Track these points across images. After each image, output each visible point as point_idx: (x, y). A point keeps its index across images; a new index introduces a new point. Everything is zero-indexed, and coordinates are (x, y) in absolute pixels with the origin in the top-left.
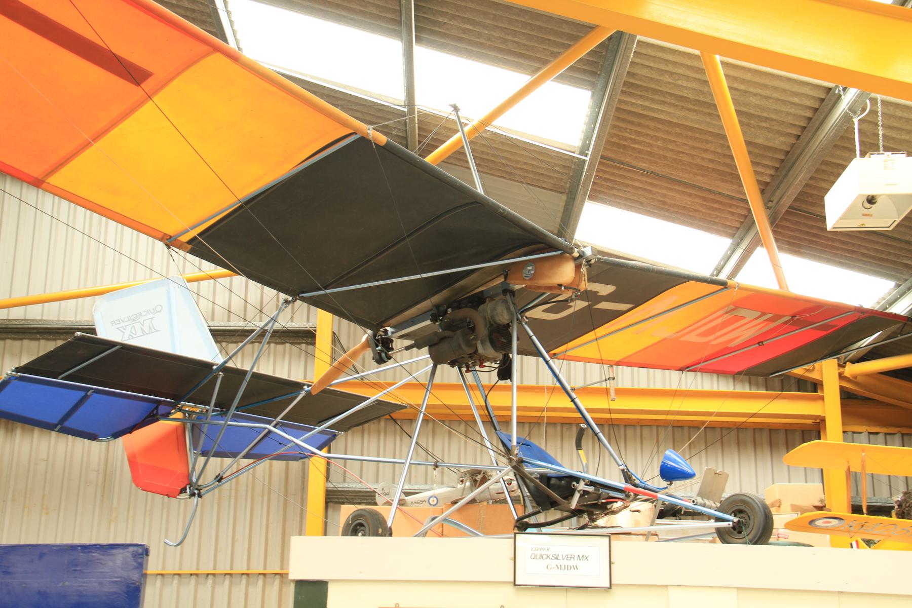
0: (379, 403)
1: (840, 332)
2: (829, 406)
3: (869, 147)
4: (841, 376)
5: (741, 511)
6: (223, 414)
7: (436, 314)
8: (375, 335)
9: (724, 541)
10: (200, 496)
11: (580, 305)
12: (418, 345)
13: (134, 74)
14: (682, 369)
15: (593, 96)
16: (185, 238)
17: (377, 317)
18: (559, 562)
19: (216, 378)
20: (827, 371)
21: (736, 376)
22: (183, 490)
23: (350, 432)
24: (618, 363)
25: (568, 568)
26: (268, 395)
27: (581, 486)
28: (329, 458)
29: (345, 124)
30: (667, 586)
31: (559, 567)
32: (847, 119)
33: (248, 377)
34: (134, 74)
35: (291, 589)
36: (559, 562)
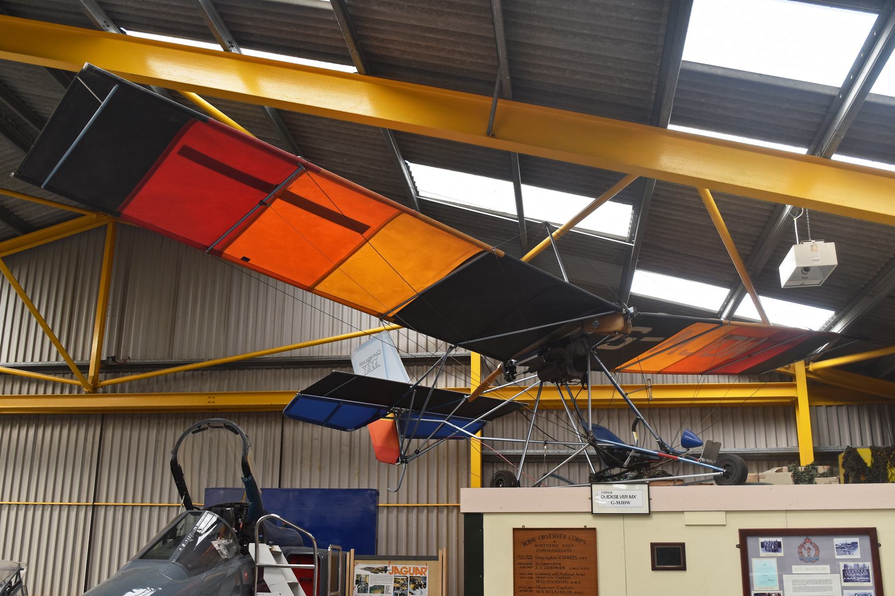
0: (512, 403)
1: (802, 344)
2: (801, 393)
3: (804, 238)
4: (807, 371)
5: (728, 465)
6: (417, 415)
7: (542, 351)
8: (505, 365)
9: (719, 484)
10: (407, 462)
11: (629, 340)
12: (531, 371)
13: (360, 228)
14: (702, 374)
15: (633, 208)
16: (391, 315)
17: (504, 355)
18: (618, 500)
19: (412, 392)
20: (799, 368)
21: (742, 374)
22: (398, 461)
23: (494, 421)
24: (659, 373)
25: (623, 503)
26: (444, 401)
27: (631, 454)
28: (482, 440)
29: (479, 246)
30: (683, 512)
31: (618, 503)
32: (790, 218)
33: (431, 392)
34: (360, 228)
35: (462, 517)
36: (618, 500)
